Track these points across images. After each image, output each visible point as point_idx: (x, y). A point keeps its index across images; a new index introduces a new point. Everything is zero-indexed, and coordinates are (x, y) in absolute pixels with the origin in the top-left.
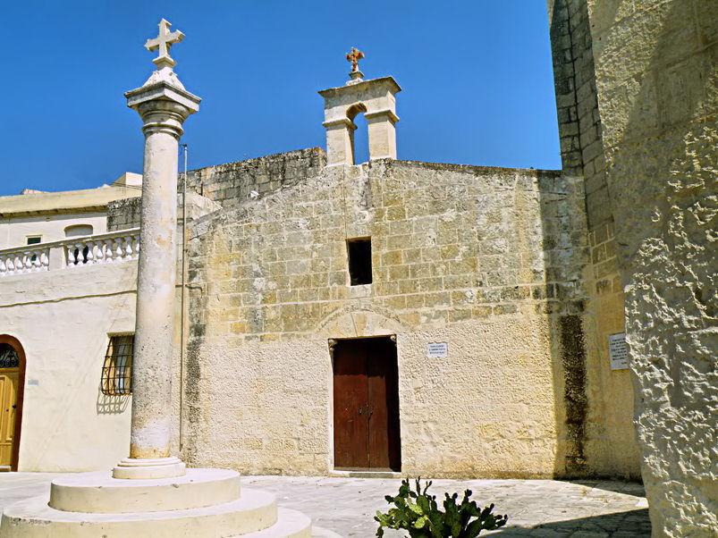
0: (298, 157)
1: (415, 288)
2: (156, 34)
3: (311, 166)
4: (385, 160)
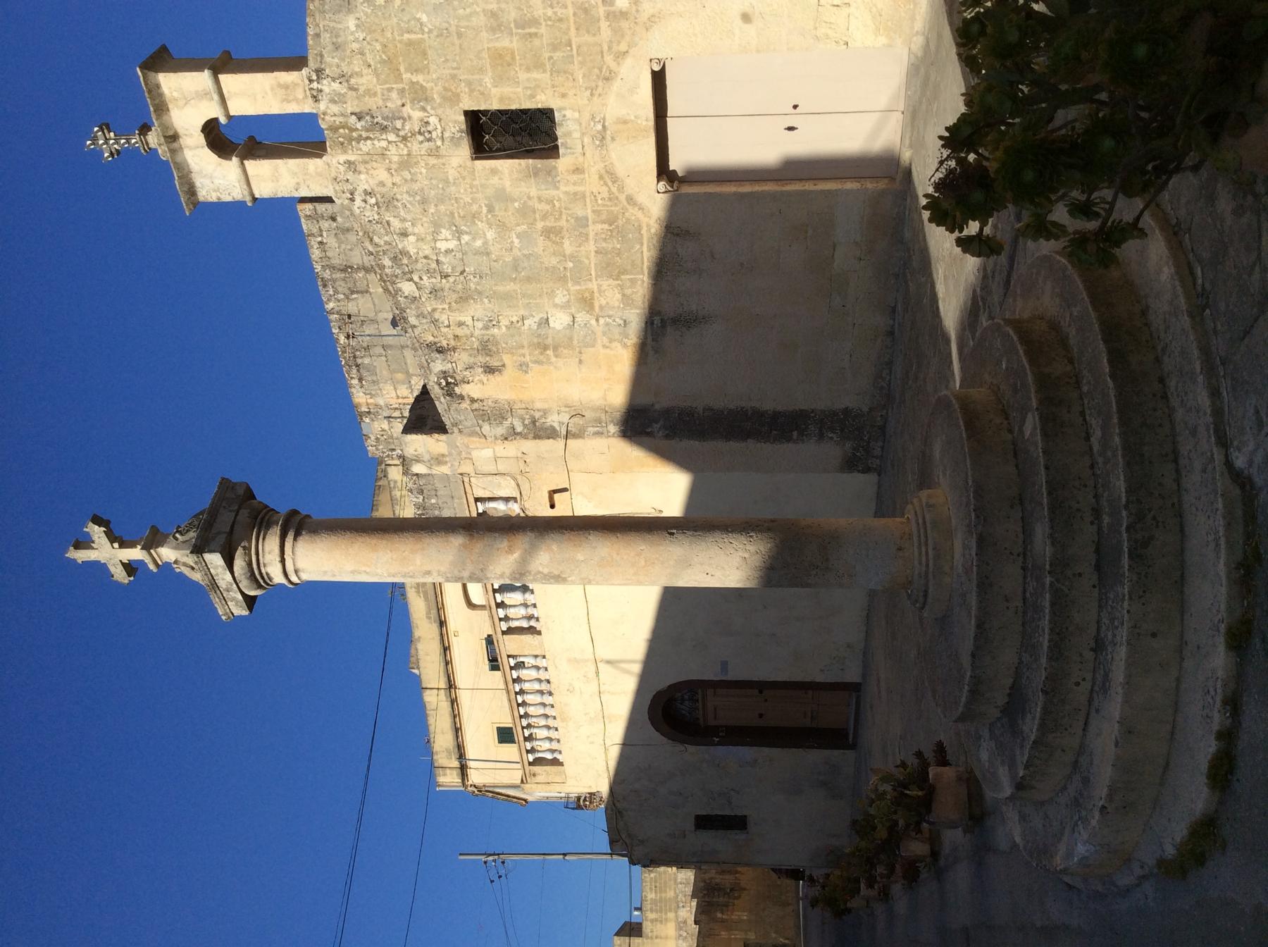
0: (321, 243)
1: (560, 20)
2: (99, 568)
3: (334, 219)
4: (311, 81)
